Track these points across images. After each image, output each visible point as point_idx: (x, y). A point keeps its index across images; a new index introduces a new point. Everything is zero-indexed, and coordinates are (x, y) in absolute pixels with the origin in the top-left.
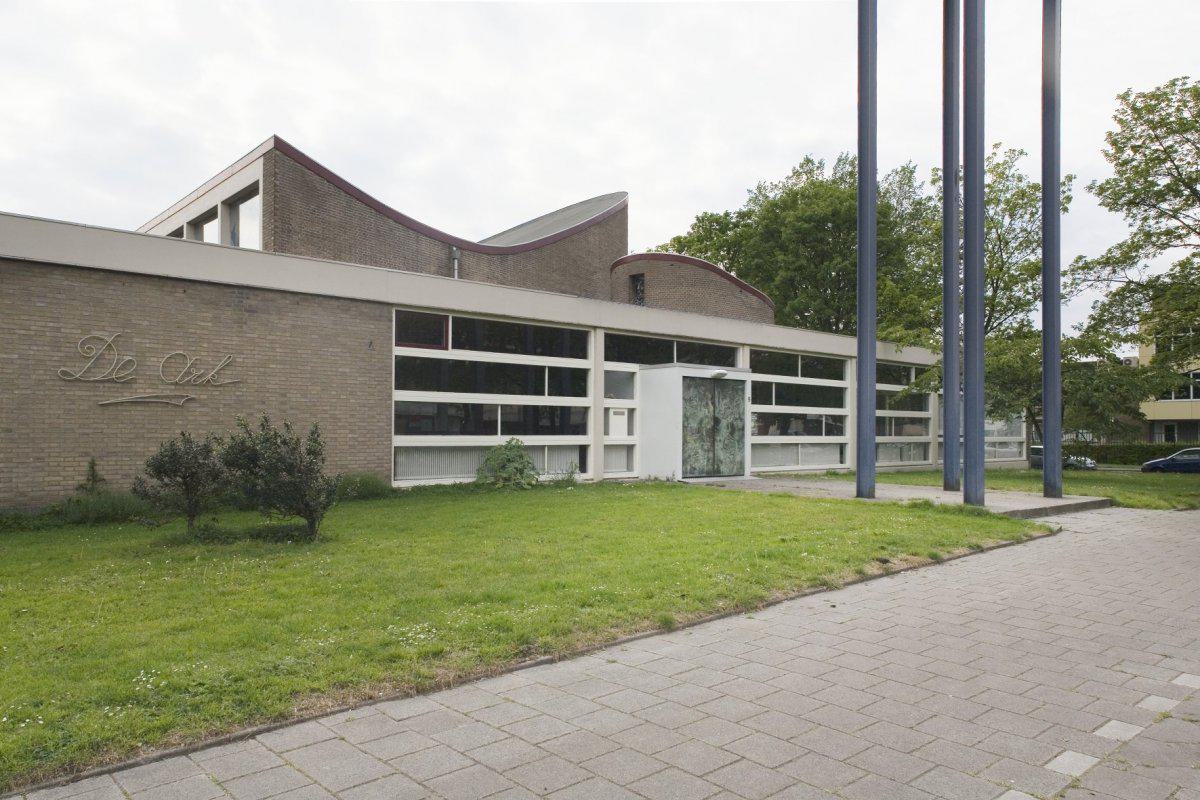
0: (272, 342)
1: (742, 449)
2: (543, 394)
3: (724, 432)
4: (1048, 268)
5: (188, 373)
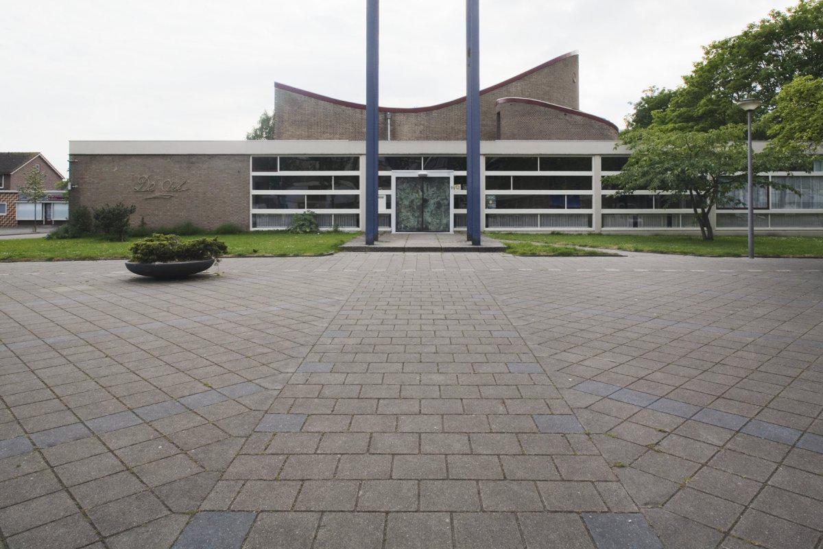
0: (200, 174)
2: (510, 189)
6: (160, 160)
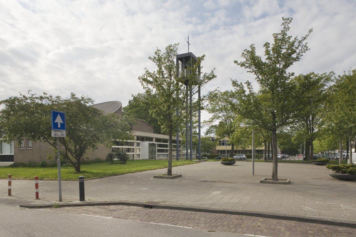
1: (156, 155)
4: (199, 121)
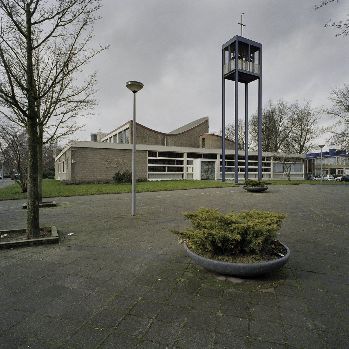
3: (210, 171)
5: (117, 163)
6: (113, 151)
